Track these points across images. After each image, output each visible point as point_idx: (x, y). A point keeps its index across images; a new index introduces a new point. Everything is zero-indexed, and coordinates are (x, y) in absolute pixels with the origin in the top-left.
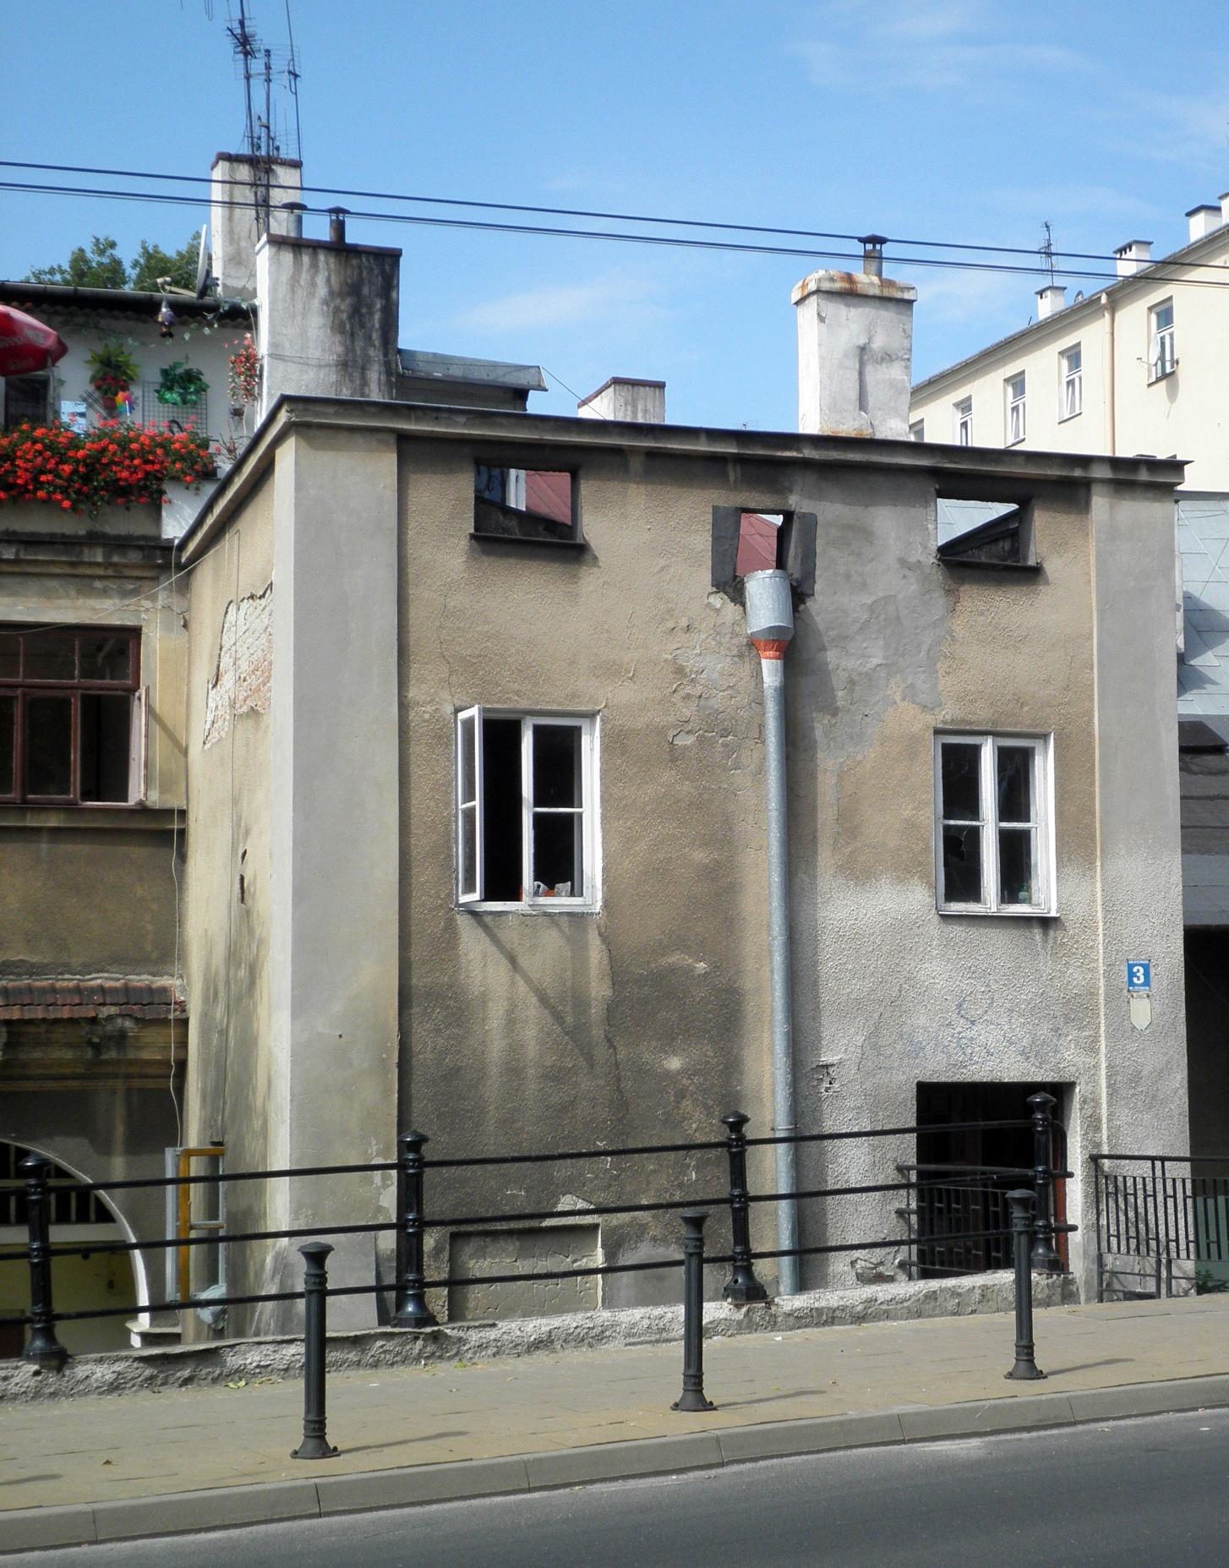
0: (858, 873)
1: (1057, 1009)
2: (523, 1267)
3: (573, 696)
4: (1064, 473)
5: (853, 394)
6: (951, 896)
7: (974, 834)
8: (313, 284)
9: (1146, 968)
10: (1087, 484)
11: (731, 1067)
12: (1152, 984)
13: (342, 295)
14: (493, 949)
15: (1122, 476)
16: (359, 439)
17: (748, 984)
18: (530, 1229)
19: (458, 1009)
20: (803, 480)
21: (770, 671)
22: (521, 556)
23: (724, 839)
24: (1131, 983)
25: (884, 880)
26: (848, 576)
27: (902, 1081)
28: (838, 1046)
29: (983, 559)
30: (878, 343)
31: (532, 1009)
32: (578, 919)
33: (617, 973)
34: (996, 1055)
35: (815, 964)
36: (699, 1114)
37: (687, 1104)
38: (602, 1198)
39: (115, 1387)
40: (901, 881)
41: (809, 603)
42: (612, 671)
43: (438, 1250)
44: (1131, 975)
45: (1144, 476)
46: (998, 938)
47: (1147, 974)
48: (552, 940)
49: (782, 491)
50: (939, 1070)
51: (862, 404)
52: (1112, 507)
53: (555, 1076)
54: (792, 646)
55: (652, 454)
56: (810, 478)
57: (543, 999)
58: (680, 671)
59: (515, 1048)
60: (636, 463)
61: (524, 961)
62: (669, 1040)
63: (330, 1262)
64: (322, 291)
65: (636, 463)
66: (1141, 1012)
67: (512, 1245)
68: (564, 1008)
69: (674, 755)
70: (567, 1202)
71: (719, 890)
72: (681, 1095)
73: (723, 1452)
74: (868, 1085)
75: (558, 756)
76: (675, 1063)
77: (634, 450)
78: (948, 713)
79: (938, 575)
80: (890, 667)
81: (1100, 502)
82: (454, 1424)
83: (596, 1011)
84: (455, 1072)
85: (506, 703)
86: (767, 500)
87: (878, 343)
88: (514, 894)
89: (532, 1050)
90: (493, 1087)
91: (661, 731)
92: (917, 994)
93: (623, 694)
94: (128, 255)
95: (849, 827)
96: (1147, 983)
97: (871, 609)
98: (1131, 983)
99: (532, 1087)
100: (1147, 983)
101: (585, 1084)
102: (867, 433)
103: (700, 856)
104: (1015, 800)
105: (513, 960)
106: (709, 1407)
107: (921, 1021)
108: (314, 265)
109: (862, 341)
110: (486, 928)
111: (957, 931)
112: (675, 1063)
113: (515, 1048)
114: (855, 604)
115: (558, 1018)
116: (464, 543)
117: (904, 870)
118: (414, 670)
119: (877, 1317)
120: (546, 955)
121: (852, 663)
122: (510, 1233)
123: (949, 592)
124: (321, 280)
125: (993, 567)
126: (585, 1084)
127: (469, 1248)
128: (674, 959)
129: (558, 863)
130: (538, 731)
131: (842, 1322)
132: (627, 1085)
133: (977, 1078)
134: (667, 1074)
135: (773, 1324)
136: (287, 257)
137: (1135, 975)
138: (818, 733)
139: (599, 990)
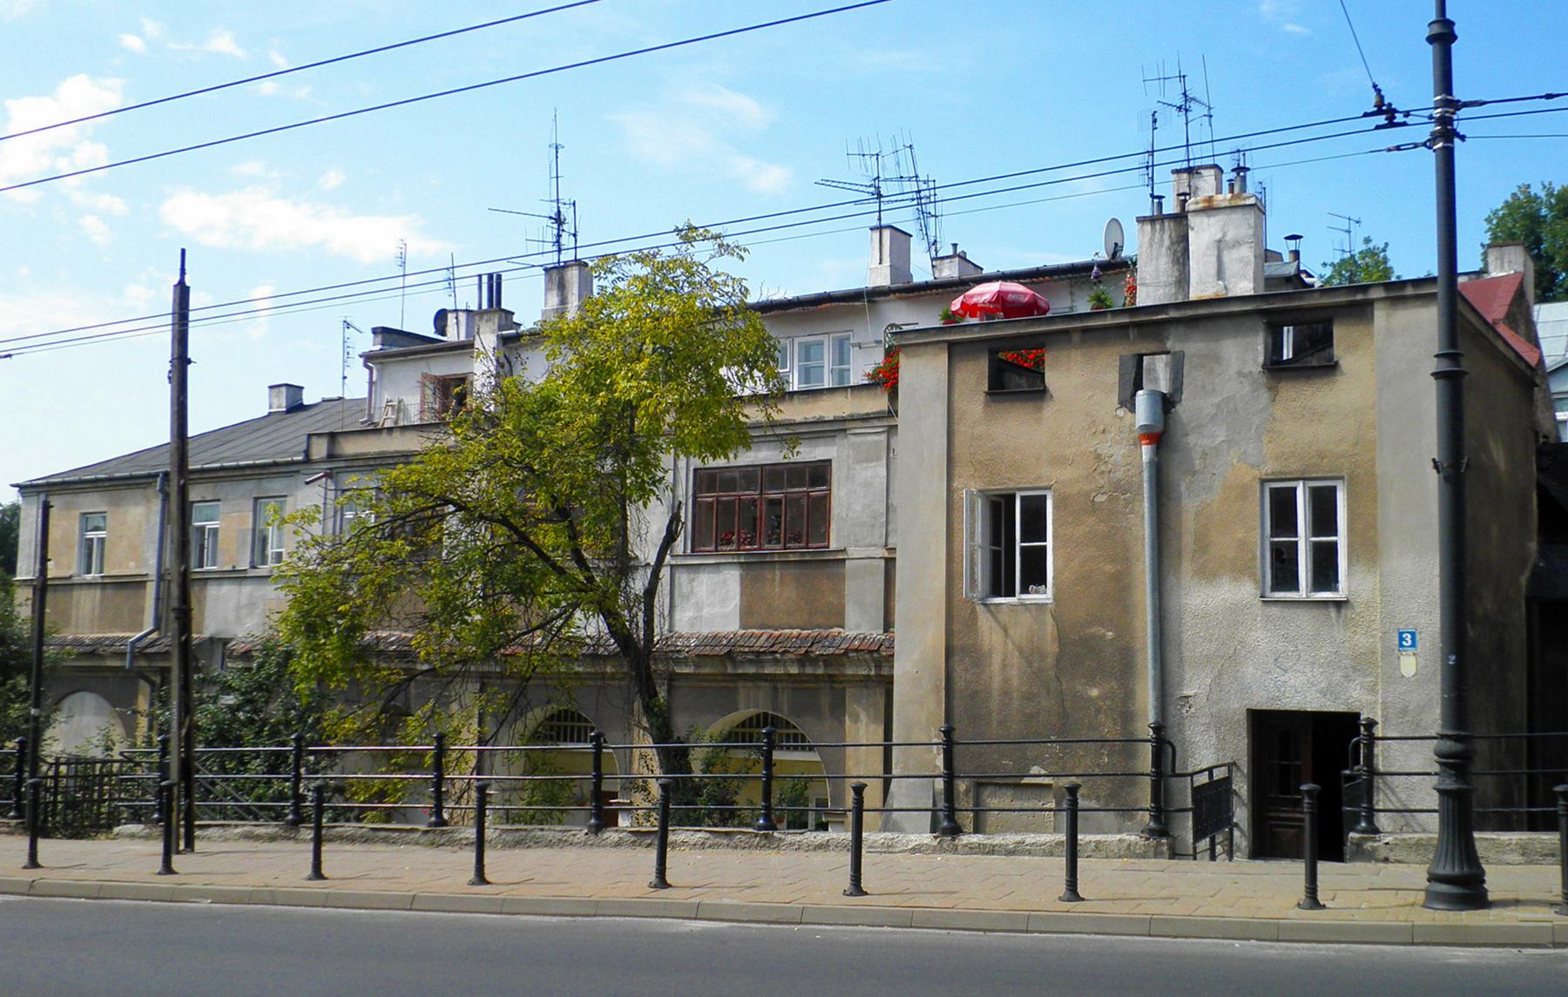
0: (1208, 574)
1: (1347, 662)
2: (1017, 805)
3: (1039, 478)
4: (1350, 298)
5: (1213, 271)
6: (1276, 587)
7: (1333, 547)
8: (1162, 240)
9: (1413, 635)
10: (1370, 304)
11: (1128, 695)
12: (1419, 645)
13: (1178, 243)
14: (994, 625)
15: (1392, 294)
16: (929, 349)
17: (1138, 646)
18: (1015, 784)
19: (978, 658)
20: (1174, 332)
21: (1146, 452)
22: (1320, 376)
23: (1124, 558)
24: (1401, 645)
25: (1225, 579)
26: (1204, 387)
27: (1237, 707)
28: (1194, 685)
29: (1315, 364)
30: (1230, 236)
31: (1015, 659)
32: (1040, 607)
33: (1061, 638)
34: (1303, 690)
35: (1180, 633)
36: (1109, 723)
37: (1102, 717)
38: (1054, 769)
39: (618, 844)
40: (1236, 579)
41: (1178, 407)
42: (1060, 461)
43: (967, 792)
44: (1401, 639)
45: (1409, 291)
46: (1305, 617)
47: (1413, 639)
48: (1026, 618)
49: (1162, 340)
50: (1262, 702)
51: (1220, 274)
52: (1388, 316)
53: (1028, 697)
54: (1160, 438)
55: (1085, 330)
56: (1181, 329)
57: (1020, 651)
58: (1098, 457)
59: (1006, 680)
60: (1076, 337)
61: (1011, 632)
62: (1091, 680)
63: (866, 793)
64: (1167, 243)
65: (1076, 337)
66: (1408, 665)
67: (1009, 792)
68: (1030, 655)
69: (1094, 508)
70: (1035, 770)
71: (1121, 585)
72: (1098, 711)
73: (326, 901)
74: (1214, 710)
75: (1035, 511)
76: (1094, 692)
77: (1075, 330)
78: (1269, 468)
79: (1263, 380)
80: (1230, 442)
81: (1380, 314)
82: (754, 883)
83: (1050, 660)
84: (975, 694)
85: (1001, 485)
86: (1152, 347)
87: (1230, 236)
88: (1011, 593)
89: (1015, 682)
90: (994, 704)
91: (1087, 494)
92: (1248, 654)
93: (1066, 474)
94: (1537, 190)
95: (1202, 544)
96: (1413, 645)
97: (1218, 406)
98: (1401, 645)
99: (1016, 703)
100: (1413, 645)
101: (1045, 703)
102: (1222, 294)
103: (1109, 568)
104: (1324, 519)
105: (1006, 630)
106: (324, 878)
107: (1249, 671)
108: (1162, 229)
109: (1218, 236)
110: (989, 611)
111: (1275, 610)
112: (1094, 692)
113: (1006, 680)
114: (1208, 405)
115: (1030, 664)
116: (982, 397)
117: (1240, 570)
118: (957, 471)
119: (1023, 853)
120: (1022, 628)
121: (1206, 442)
122: (1008, 785)
123: (1270, 389)
124: (1166, 237)
125: (1314, 368)
126: (1045, 703)
127: (987, 792)
128: (1093, 630)
129: (1035, 574)
130: (1023, 499)
131: (999, 853)
132: (1068, 704)
133: (1288, 708)
134: (1090, 699)
135: (955, 850)
136: (1148, 227)
137: (1406, 639)
138: (1183, 488)
139: (1052, 648)
